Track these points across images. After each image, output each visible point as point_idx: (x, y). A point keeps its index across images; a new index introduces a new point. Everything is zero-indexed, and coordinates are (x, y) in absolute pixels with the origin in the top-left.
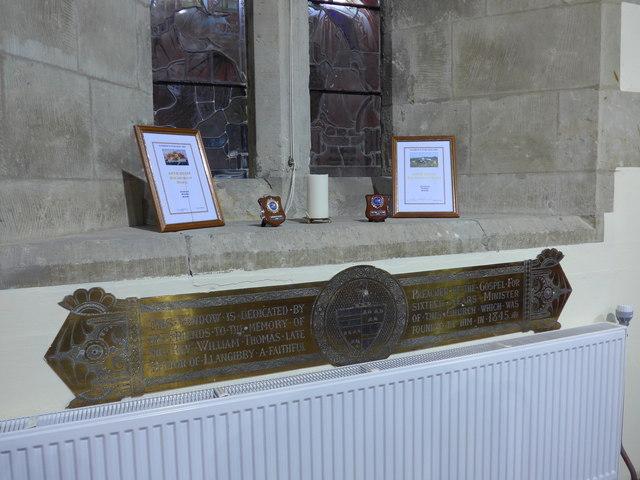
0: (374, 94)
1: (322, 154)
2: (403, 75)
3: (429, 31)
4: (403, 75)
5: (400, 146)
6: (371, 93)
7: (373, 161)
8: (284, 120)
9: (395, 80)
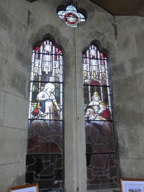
0: (112, 153)
1: (92, 179)
2: (123, 147)
3: (132, 131)
4: (123, 147)
5: (123, 183)
6: (111, 153)
7: (114, 181)
8: (75, 171)
9: (120, 149)
